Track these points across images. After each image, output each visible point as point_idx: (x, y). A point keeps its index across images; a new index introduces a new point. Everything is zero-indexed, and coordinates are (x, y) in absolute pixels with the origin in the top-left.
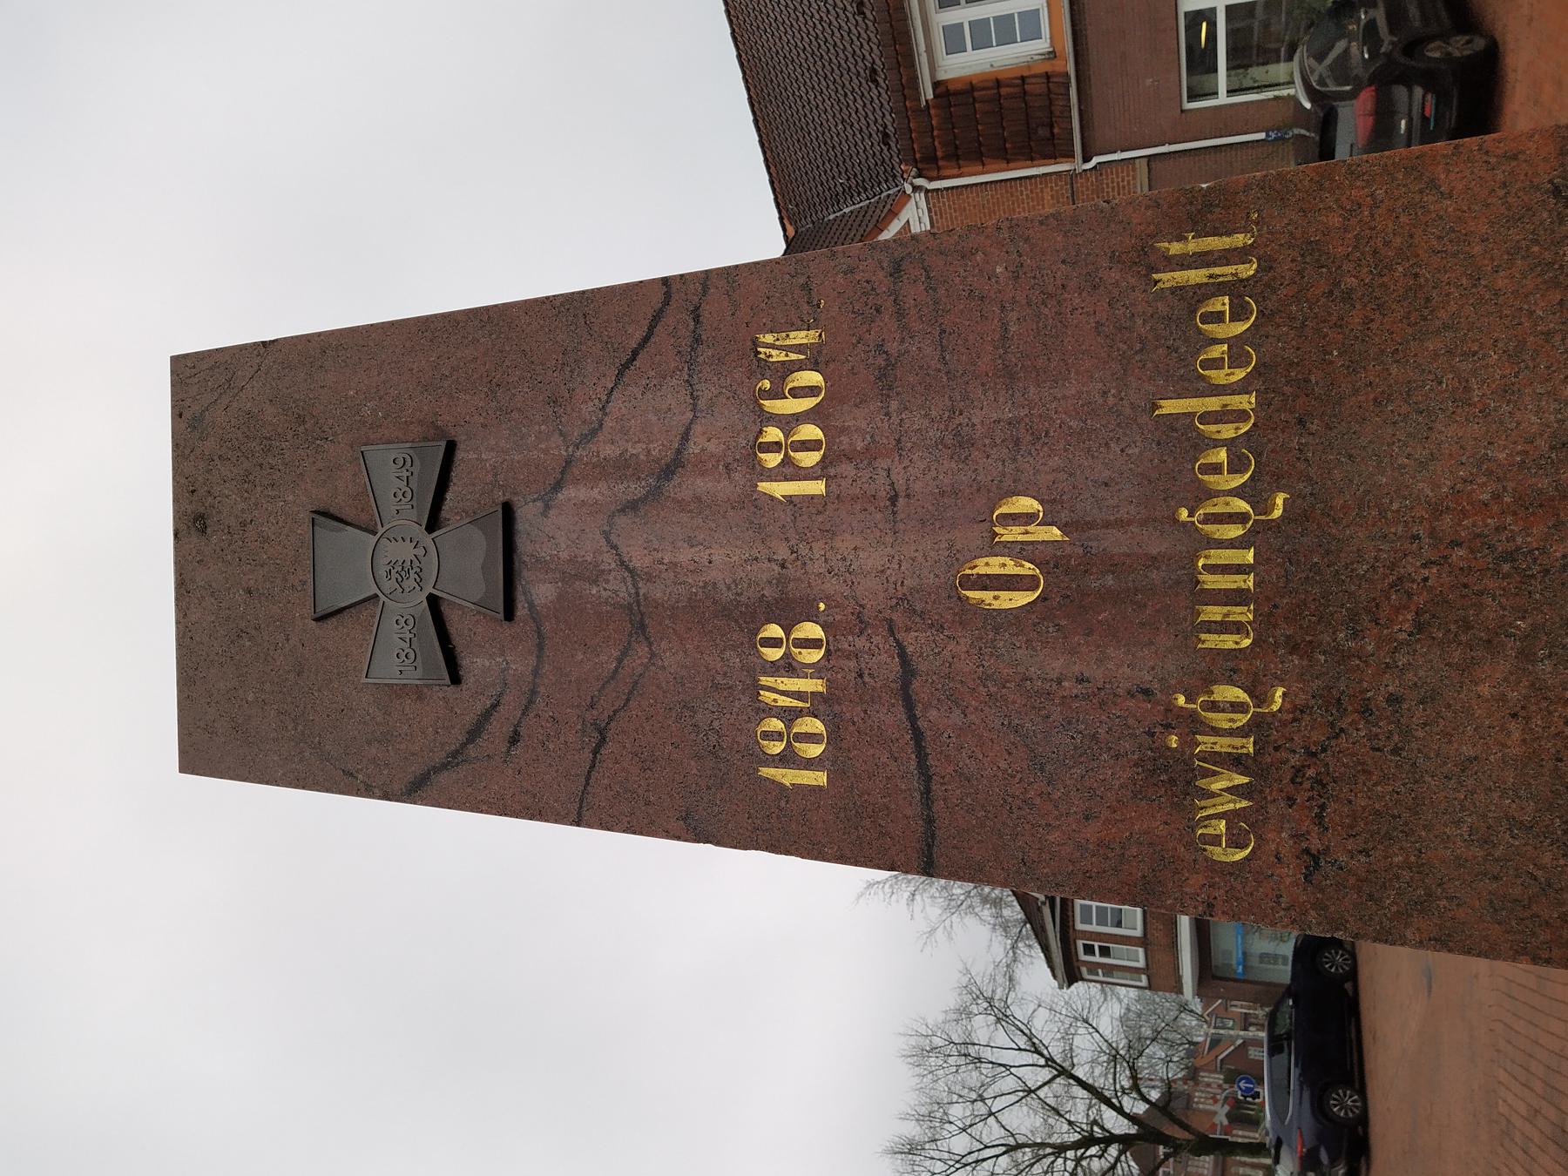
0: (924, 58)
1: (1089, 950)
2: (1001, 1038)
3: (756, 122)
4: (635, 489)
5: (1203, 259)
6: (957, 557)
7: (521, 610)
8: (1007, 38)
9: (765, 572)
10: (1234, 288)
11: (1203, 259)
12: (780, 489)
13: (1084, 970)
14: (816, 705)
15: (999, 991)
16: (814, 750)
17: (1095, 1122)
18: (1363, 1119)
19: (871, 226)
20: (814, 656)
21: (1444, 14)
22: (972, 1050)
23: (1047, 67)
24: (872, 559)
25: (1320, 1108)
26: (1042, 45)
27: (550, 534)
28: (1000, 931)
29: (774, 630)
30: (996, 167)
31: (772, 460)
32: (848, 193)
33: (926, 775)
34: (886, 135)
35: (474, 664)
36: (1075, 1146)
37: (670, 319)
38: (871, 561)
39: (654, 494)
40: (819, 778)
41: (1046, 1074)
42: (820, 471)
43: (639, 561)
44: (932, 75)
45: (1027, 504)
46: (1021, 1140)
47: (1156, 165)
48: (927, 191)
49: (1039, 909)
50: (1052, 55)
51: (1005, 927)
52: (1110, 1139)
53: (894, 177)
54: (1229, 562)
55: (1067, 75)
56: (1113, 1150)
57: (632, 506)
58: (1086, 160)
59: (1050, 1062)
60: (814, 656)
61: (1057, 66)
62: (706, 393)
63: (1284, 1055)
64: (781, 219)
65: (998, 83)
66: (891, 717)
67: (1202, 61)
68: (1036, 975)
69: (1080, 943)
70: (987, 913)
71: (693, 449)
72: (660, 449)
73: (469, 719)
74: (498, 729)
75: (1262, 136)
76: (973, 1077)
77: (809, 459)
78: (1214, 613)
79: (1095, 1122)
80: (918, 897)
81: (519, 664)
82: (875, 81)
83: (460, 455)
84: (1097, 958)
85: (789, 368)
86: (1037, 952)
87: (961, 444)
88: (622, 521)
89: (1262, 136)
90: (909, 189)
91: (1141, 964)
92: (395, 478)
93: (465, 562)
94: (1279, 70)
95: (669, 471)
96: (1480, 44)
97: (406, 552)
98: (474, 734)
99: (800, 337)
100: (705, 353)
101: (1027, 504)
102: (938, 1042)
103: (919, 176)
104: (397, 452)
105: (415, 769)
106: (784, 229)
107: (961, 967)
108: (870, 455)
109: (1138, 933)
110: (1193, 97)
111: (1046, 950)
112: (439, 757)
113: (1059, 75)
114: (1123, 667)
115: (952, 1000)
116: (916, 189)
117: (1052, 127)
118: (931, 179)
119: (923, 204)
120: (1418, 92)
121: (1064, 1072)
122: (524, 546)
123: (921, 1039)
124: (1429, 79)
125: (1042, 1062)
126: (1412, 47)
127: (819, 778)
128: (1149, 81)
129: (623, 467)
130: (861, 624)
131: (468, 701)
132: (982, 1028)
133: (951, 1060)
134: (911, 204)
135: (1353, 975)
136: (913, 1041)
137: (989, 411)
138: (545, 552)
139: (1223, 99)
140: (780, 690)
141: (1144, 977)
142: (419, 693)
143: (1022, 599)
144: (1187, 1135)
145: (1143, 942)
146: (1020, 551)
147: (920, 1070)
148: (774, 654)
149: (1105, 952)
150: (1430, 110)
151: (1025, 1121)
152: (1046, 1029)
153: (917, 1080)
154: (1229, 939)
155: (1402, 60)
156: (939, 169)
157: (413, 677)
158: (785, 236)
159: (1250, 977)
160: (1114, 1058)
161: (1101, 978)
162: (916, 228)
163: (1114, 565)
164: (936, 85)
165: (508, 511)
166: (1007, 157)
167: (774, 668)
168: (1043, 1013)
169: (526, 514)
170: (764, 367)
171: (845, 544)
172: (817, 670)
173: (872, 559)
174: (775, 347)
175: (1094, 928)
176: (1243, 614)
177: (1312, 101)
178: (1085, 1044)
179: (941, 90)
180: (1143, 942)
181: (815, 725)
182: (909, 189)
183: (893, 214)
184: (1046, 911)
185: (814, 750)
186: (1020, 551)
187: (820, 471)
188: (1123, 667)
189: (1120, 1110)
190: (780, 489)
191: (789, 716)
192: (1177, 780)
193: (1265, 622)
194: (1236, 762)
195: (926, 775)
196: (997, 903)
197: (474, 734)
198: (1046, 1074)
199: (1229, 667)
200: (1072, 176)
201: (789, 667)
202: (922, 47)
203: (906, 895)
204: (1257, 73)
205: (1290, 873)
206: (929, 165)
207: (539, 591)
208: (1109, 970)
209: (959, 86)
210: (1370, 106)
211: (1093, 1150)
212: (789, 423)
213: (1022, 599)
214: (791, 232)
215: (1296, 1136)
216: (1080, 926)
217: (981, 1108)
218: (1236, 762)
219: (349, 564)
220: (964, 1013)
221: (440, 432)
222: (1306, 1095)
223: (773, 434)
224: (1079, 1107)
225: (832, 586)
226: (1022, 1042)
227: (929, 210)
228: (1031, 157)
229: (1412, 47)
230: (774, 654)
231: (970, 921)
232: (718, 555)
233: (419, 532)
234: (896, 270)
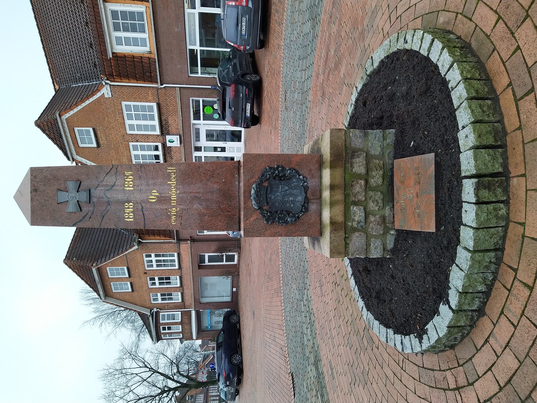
0: (109, 45)
1: (164, 329)
2: (134, 365)
3: (44, 48)
4: (108, 188)
5: (171, 170)
6: (148, 196)
7: (91, 202)
8: (136, 45)
9: (126, 197)
10: (174, 172)
11: (171, 170)
12: (128, 189)
13: (162, 336)
14: (132, 212)
15: (134, 349)
16: (131, 217)
17: (166, 386)
18: (242, 362)
19: (90, 93)
20: (132, 207)
21: (251, 68)
22: (124, 371)
23: (149, 55)
24: (138, 196)
25: (230, 362)
26: (147, 49)
27: (97, 193)
28: (134, 331)
29: (127, 204)
30: (133, 81)
31: (126, 185)
32: (81, 80)
33: (144, 218)
34: (95, 65)
35: (84, 209)
36: (159, 394)
37: (113, 169)
38: (138, 197)
39: (111, 189)
40: (132, 220)
41: (149, 374)
42: (133, 187)
43: (109, 196)
44: (112, 50)
45: (155, 191)
46: (140, 397)
47: (182, 90)
48: (110, 85)
49: (148, 318)
50: (150, 52)
51: (136, 329)
52: (170, 389)
53: (98, 78)
54: (174, 197)
55: (155, 59)
56: (171, 393)
57: (108, 190)
58: (161, 85)
59: (151, 369)
60: (132, 207)
61: (152, 56)
62: (118, 178)
63: (221, 351)
64: (53, 82)
65: (133, 57)
66: (141, 213)
67: (194, 63)
68: (147, 342)
69: (161, 327)
70: (129, 326)
71: (116, 184)
72: (112, 184)
73: (83, 216)
74: (88, 216)
75: (210, 87)
76: (123, 380)
77: (131, 186)
78: (172, 202)
79: (166, 386)
80: (103, 324)
81: (91, 209)
82: (91, 47)
83: (82, 183)
84: (167, 331)
85: (128, 176)
86: (148, 336)
87: (148, 185)
88: (106, 192)
89: (210, 87)
90: (104, 84)
91: (181, 330)
92: (71, 185)
93: (83, 196)
94: (215, 70)
95: (113, 186)
96: (258, 78)
97: (74, 195)
98: (84, 217)
99: (130, 173)
100: (118, 173)
101: (155, 191)
102: (111, 371)
103: (108, 80)
104: (71, 182)
105: (74, 223)
106: (54, 86)
107: (120, 343)
108: (138, 186)
109: (180, 321)
110: (191, 73)
111: (150, 332)
112: (78, 221)
113: (152, 59)
114: (165, 207)
115: (117, 355)
116: (106, 83)
117: (151, 73)
118: (111, 81)
119: (109, 89)
120: (244, 88)
121: (155, 372)
122: (92, 194)
123: (105, 371)
124: (247, 85)
125: (148, 370)
126: (243, 75)
127: (132, 220)
128: (179, 66)
129: (107, 185)
130: (137, 203)
131: (83, 214)
132: (128, 363)
133: (116, 376)
134: (104, 89)
135: (239, 322)
136: (102, 372)
137: (151, 182)
138: (95, 195)
139: (199, 75)
140: (127, 211)
141: (181, 335)
142: (75, 213)
143: (154, 200)
144: (193, 383)
145: (181, 323)
146: (154, 196)
147: (104, 382)
148: (127, 207)
149: (169, 328)
150: (247, 93)
151: (143, 390)
152: (149, 358)
153: (104, 385)
154: (206, 323)
155: (242, 79)
156: (114, 78)
157: (75, 211)
158: (55, 89)
159: (213, 329)
160: (172, 363)
161: (168, 338)
162: (106, 96)
163: (163, 197)
164: (113, 53)
165: (90, 190)
166: (137, 80)
167: (127, 208)
168: (148, 354)
169: (92, 191)
170: (125, 175)
171: (135, 195)
172: (132, 208)
173: (138, 196)
174: (127, 173)
175: (166, 321)
176: (175, 202)
177: (220, 84)
178: (163, 361)
179: (115, 55)
180: (181, 323)
181: (132, 214)
182: (104, 84)
183: (98, 90)
184: (150, 318)
185: (131, 217)
186: (154, 196)
187: (133, 187)
188: (165, 207)
189: (173, 380)
190: (128, 189)
191: (129, 213)
192: (170, 217)
193: (177, 202)
194: (175, 215)
195: (144, 218)
196: (133, 322)
197: (84, 217)
198: (149, 374)
199: (174, 206)
200: (158, 89)
201: (129, 208)
202: (108, 41)
203: (99, 324)
204: (209, 69)
205: (179, 225)
206: (110, 77)
207: (94, 200)
208: (170, 334)
209: (121, 55)
210: (234, 89)
211: (165, 395)
212: (129, 182)
213: (154, 200)
214: (57, 87)
215: (224, 373)
216: (161, 322)
217: (127, 390)
218: (175, 215)
219: (63, 196)
220: (121, 359)
221: (79, 180)
222: (226, 360)
223: (126, 183)
224: (161, 382)
225: (134, 199)
226: (141, 364)
227: (111, 91)
228: (145, 81)
229: (243, 75)
230: (127, 207)
231: (123, 329)
232: (119, 196)
233: (76, 192)
234: (141, 167)
